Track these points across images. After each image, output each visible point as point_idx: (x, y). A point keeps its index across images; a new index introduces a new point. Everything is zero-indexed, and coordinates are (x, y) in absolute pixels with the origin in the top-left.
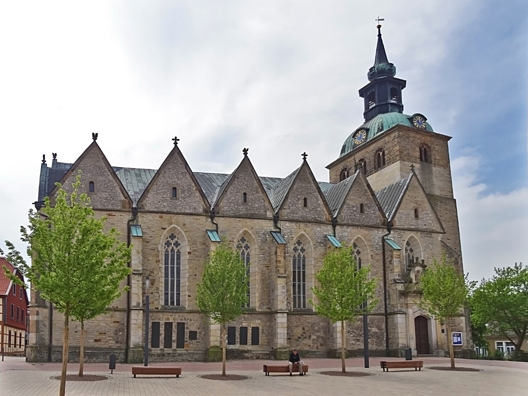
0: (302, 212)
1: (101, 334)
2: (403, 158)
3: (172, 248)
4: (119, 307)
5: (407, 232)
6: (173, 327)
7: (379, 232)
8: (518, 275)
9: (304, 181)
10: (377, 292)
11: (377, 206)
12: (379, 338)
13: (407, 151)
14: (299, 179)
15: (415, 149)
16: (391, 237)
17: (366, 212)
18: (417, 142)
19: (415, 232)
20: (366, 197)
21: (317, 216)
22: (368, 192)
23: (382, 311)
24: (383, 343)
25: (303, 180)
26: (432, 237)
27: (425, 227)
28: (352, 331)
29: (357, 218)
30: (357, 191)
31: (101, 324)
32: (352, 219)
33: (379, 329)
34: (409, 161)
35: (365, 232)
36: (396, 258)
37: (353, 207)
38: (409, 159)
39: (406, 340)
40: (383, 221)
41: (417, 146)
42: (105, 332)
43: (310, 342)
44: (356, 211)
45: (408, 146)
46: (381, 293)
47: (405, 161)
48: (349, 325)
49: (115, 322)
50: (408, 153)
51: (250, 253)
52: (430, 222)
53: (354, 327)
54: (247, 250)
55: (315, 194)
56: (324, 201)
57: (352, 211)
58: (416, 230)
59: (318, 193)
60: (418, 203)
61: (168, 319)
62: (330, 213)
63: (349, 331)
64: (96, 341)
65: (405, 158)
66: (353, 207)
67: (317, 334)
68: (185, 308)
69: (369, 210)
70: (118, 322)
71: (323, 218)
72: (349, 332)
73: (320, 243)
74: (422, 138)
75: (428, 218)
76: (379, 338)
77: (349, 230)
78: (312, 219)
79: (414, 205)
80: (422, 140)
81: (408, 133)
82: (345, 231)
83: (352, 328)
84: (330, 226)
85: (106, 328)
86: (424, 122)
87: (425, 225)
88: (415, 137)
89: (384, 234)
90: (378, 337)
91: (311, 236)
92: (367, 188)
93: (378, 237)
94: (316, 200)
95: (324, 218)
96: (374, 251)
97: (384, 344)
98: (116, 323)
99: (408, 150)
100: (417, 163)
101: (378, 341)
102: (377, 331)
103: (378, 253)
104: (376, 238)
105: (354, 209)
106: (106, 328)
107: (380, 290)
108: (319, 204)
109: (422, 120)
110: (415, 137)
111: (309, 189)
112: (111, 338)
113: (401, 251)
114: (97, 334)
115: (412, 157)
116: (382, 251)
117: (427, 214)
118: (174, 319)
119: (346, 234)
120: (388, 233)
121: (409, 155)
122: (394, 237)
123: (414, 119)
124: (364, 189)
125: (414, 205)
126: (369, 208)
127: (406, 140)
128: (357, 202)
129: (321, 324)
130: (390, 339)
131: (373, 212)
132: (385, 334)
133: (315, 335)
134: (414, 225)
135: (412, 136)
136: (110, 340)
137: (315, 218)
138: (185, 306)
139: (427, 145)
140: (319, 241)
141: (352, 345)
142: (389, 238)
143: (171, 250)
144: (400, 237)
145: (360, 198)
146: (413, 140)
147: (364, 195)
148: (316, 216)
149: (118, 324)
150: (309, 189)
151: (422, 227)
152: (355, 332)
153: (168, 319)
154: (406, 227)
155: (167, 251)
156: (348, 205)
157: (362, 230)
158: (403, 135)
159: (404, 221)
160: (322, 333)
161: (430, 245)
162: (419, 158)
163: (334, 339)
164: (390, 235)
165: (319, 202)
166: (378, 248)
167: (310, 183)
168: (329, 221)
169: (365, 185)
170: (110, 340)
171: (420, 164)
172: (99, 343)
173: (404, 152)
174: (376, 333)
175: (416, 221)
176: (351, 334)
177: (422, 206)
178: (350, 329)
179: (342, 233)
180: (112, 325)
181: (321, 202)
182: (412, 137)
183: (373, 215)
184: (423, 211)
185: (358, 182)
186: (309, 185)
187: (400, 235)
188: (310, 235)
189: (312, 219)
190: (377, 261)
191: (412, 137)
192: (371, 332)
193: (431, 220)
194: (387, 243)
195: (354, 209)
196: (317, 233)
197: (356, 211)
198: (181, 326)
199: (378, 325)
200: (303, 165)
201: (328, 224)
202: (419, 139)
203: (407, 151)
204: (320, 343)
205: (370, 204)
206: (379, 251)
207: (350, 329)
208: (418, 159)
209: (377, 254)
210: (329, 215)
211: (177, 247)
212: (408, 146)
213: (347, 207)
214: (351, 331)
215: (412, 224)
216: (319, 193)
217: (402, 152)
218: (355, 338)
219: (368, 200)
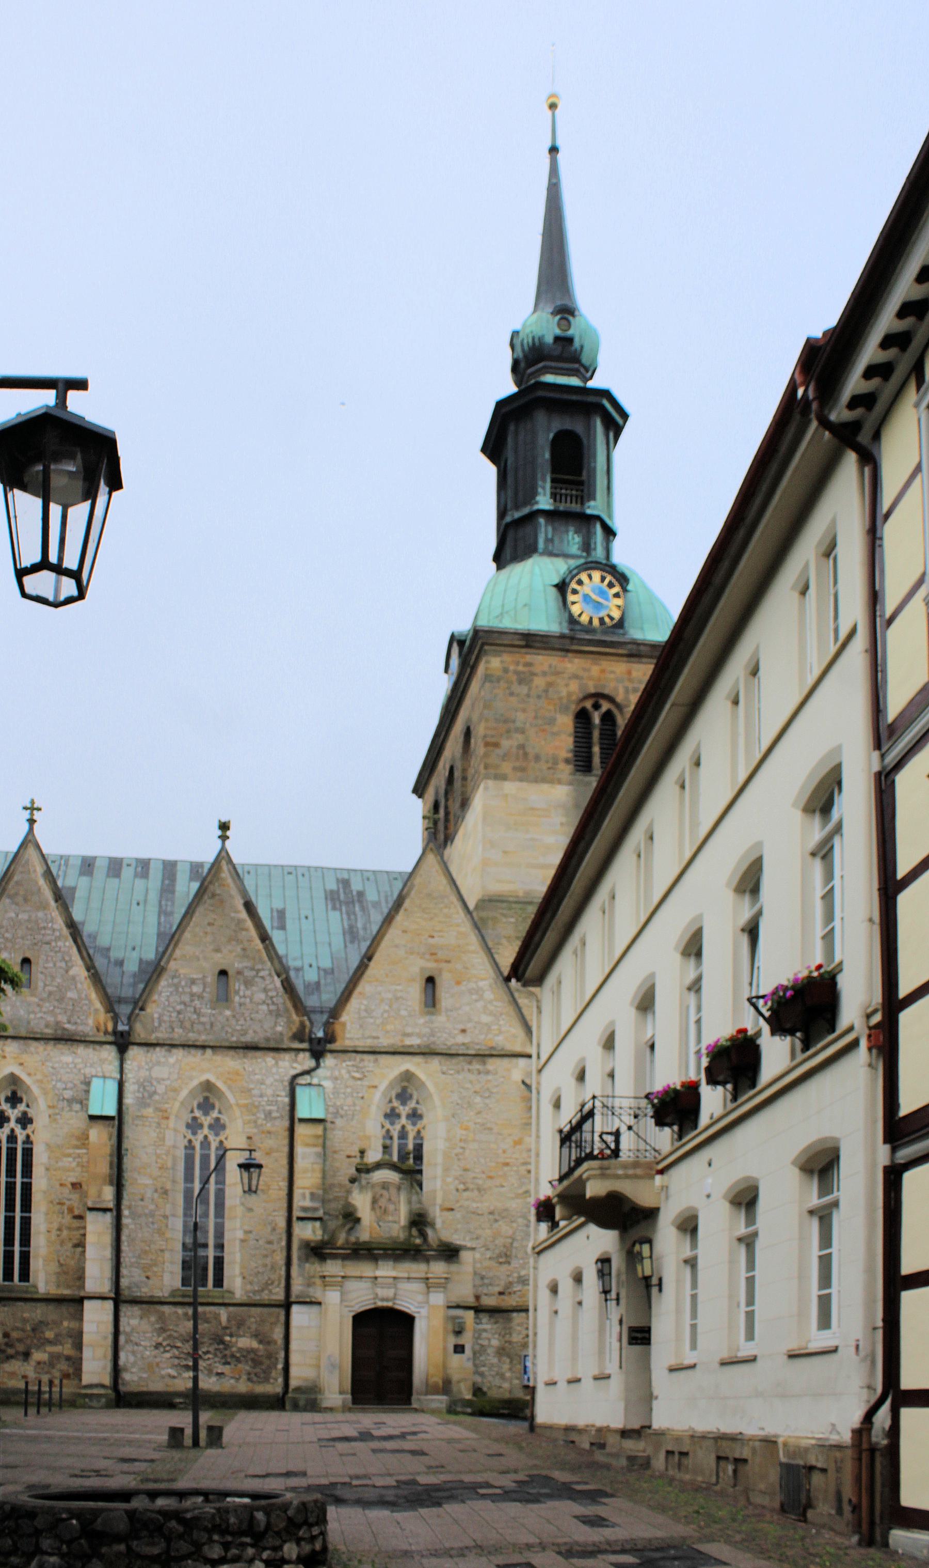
0: (13, 1006)
2: (497, 767)
3: (206, 1137)
5: (384, 1060)
7: (281, 1063)
9: (26, 900)
10: (261, 1242)
11: (279, 976)
12: (261, 1363)
13: (518, 738)
14: (10, 897)
15: (552, 721)
16: (326, 1078)
17: (237, 999)
18: (564, 693)
19: (418, 1059)
20: (239, 949)
21: (63, 1018)
22: (247, 930)
23: (276, 1294)
24: (273, 1374)
25: (20, 899)
26: (488, 1072)
27: (461, 1039)
28: (168, 1345)
29: (203, 1019)
30: (209, 929)
32: (188, 1025)
33: (260, 1342)
34: (521, 780)
35: (230, 1063)
36: (307, 1145)
37: (193, 982)
38: (523, 769)
40: (297, 1024)
41: (564, 709)
43: (29, 1369)
44: (200, 997)
45: (521, 716)
46: (275, 1246)
47: (504, 778)
48: (161, 1328)
50: (522, 747)
51: (33, 1138)
52: (485, 1019)
53: (175, 1334)
54: (24, 1128)
55: (59, 944)
56: (90, 967)
57: (186, 998)
58: (427, 1053)
59: (70, 942)
60: (441, 955)
62: (110, 1003)
63: (160, 1344)
65: (506, 767)
66: (193, 982)
67: (49, 1349)
69: (248, 993)
71: (86, 1024)
72: (158, 1346)
73: (70, 1101)
74: (589, 670)
75: (480, 1005)
76: (261, 1363)
77: (172, 1060)
78: (47, 1026)
79: (422, 963)
80: (590, 678)
81: (529, 658)
82: (159, 1063)
83: (170, 1336)
84: (108, 1047)
86: (617, 595)
87: (463, 1031)
88: (557, 673)
89: (299, 1068)
90: (256, 1362)
91: (41, 1081)
92: (244, 915)
93: (276, 1080)
94: (63, 964)
95: (91, 1022)
96: (260, 1122)
97: (276, 1380)
99: (522, 731)
100: (560, 782)
101: (258, 1370)
102: (255, 1344)
103: (274, 1129)
104: (269, 1081)
105: (196, 989)
107: (274, 1238)
108: (73, 978)
109: (611, 585)
110: (557, 673)
111: (40, 929)
115: (537, 758)
117: (478, 991)
119: (158, 1072)
120: (312, 1063)
121: (526, 754)
122: (336, 1079)
123: (574, 585)
124: (233, 919)
125: (422, 963)
126: (248, 983)
127: (516, 688)
128: (205, 964)
129: (65, 1324)
131: (262, 996)
132: (282, 1354)
133: (45, 1351)
134: (419, 1035)
135: (546, 668)
137: (57, 1023)
139: (610, 699)
140: (68, 1094)
141: (168, 1380)
142: (315, 1081)
143: (202, 1143)
144: (357, 1075)
145: (218, 950)
146: (550, 685)
147: (233, 939)
148: (60, 1018)
150: (40, 929)
151: (444, 1040)
152: (177, 1348)
154: (385, 1042)
155: (190, 1146)
156: (173, 977)
157: (215, 1057)
158: (506, 670)
159: (378, 1021)
160: (68, 1346)
161: (478, 1099)
162: (567, 761)
164: (320, 1072)
165: (71, 973)
166: (275, 1114)
167: (44, 907)
168: (106, 1033)
169: (239, 903)
171: (570, 784)
173: (506, 743)
174: (252, 1351)
175: (427, 1018)
176: (166, 1351)
177: (459, 966)
178: (164, 1339)
179: (150, 1070)
181: (79, 970)
182: (544, 674)
183: (264, 1007)
184: (458, 983)
185: (213, 895)
186: (40, 914)
187: (358, 1068)
188: (39, 1077)
189: (47, 1026)
190: (267, 1154)
191: (544, 674)
192: (234, 1349)
193: (491, 1014)
195: (196, 989)
196: (62, 1071)
197: (200, 997)
199: (256, 1330)
200: (24, 845)
201: (102, 1043)
202: (576, 677)
203: (518, 738)
204: (61, 1371)
205: (252, 969)
206: (277, 1122)
207: (164, 1339)
208: (562, 766)
209: (269, 1132)
210: (108, 1011)
211: (24, 1128)
212: (521, 716)
213: (169, 986)
214: (165, 1343)
215: (409, 1030)
216: (75, 941)
217: (496, 745)
218: (176, 1361)
219: (247, 957)
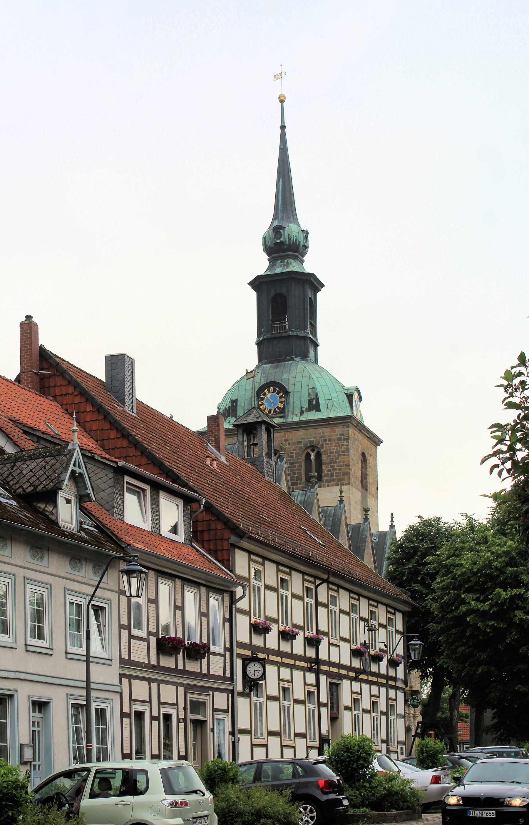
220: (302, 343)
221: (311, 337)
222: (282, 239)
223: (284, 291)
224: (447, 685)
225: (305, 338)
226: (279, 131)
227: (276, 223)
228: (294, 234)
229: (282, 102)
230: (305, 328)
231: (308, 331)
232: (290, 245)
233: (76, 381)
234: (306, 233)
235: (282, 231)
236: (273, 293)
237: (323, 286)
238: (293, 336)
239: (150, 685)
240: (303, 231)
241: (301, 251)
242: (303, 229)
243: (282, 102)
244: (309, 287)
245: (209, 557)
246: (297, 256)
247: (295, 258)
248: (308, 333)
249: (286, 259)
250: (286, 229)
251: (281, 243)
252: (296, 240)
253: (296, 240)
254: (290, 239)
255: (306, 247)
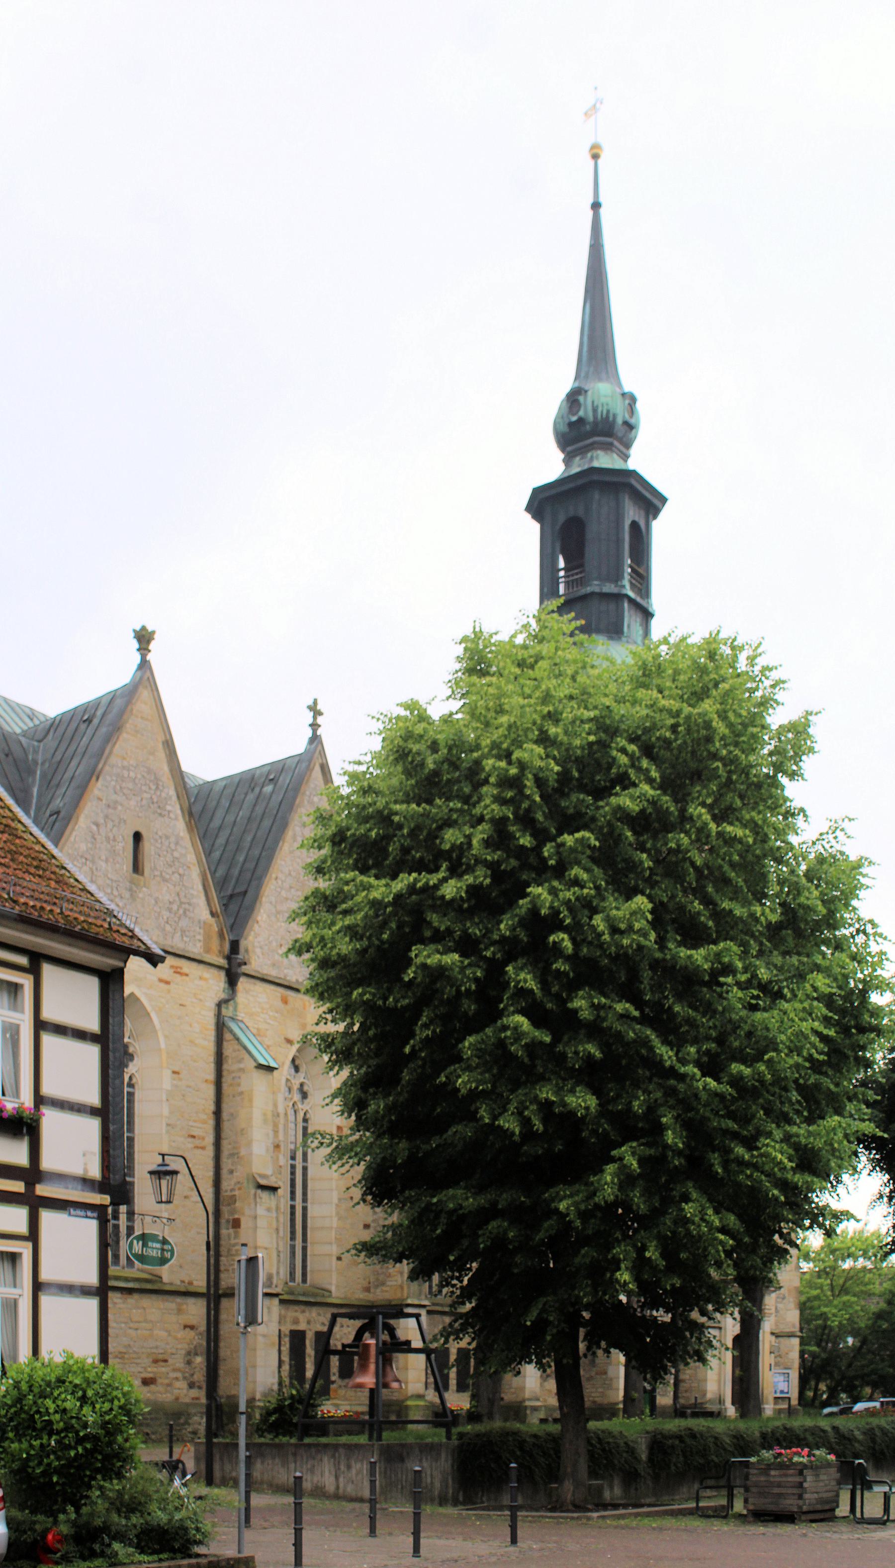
1: (156, 1361)
4: (195, 1283)
6: (308, 1342)
8: (606, 1183)
31: (155, 1332)
39: (256, 1475)
42: (166, 1357)
49: (185, 1327)
61: (296, 1321)
64: (146, 1382)
68: (330, 1292)
70: (192, 1327)
85: (167, 1344)
98: (188, 1330)
106: (167, 1344)
112: (179, 1375)
113: (275, 1072)
114: (147, 1361)
116: (225, 1067)
118: (309, 1322)
130: (683, 1381)
136: (177, 1379)
138: (327, 1287)
149: (192, 1333)
153: (296, 1321)
163: (611, 1379)
170: (177, 1379)
172: (153, 1387)
180: (179, 1336)
194: (231, 1031)
198: (324, 1338)
220: (612, 606)
221: (631, 594)
222: (581, 413)
223: (581, 512)
224: (558, 970)
225: (619, 597)
226: (590, 214)
227: (577, 385)
228: (603, 400)
229: (595, 157)
230: (617, 577)
231: (626, 582)
232: (595, 423)
233: (190, 829)
234: (631, 400)
235: (581, 399)
236: (562, 518)
237: (664, 500)
238: (593, 594)
239: (85, 1291)
240: (624, 395)
241: (620, 434)
242: (627, 389)
243: (595, 157)
244: (630, 498)
245: (34, 801)
246: (611, 444)
247: (607, 447)
248: (624, 586)
249: (589, 451)
250: (589, 393)
251: (581, 421)
252: (608, 412)
253: (608, 412)
254: (595, 410)
255: (630, 427)
